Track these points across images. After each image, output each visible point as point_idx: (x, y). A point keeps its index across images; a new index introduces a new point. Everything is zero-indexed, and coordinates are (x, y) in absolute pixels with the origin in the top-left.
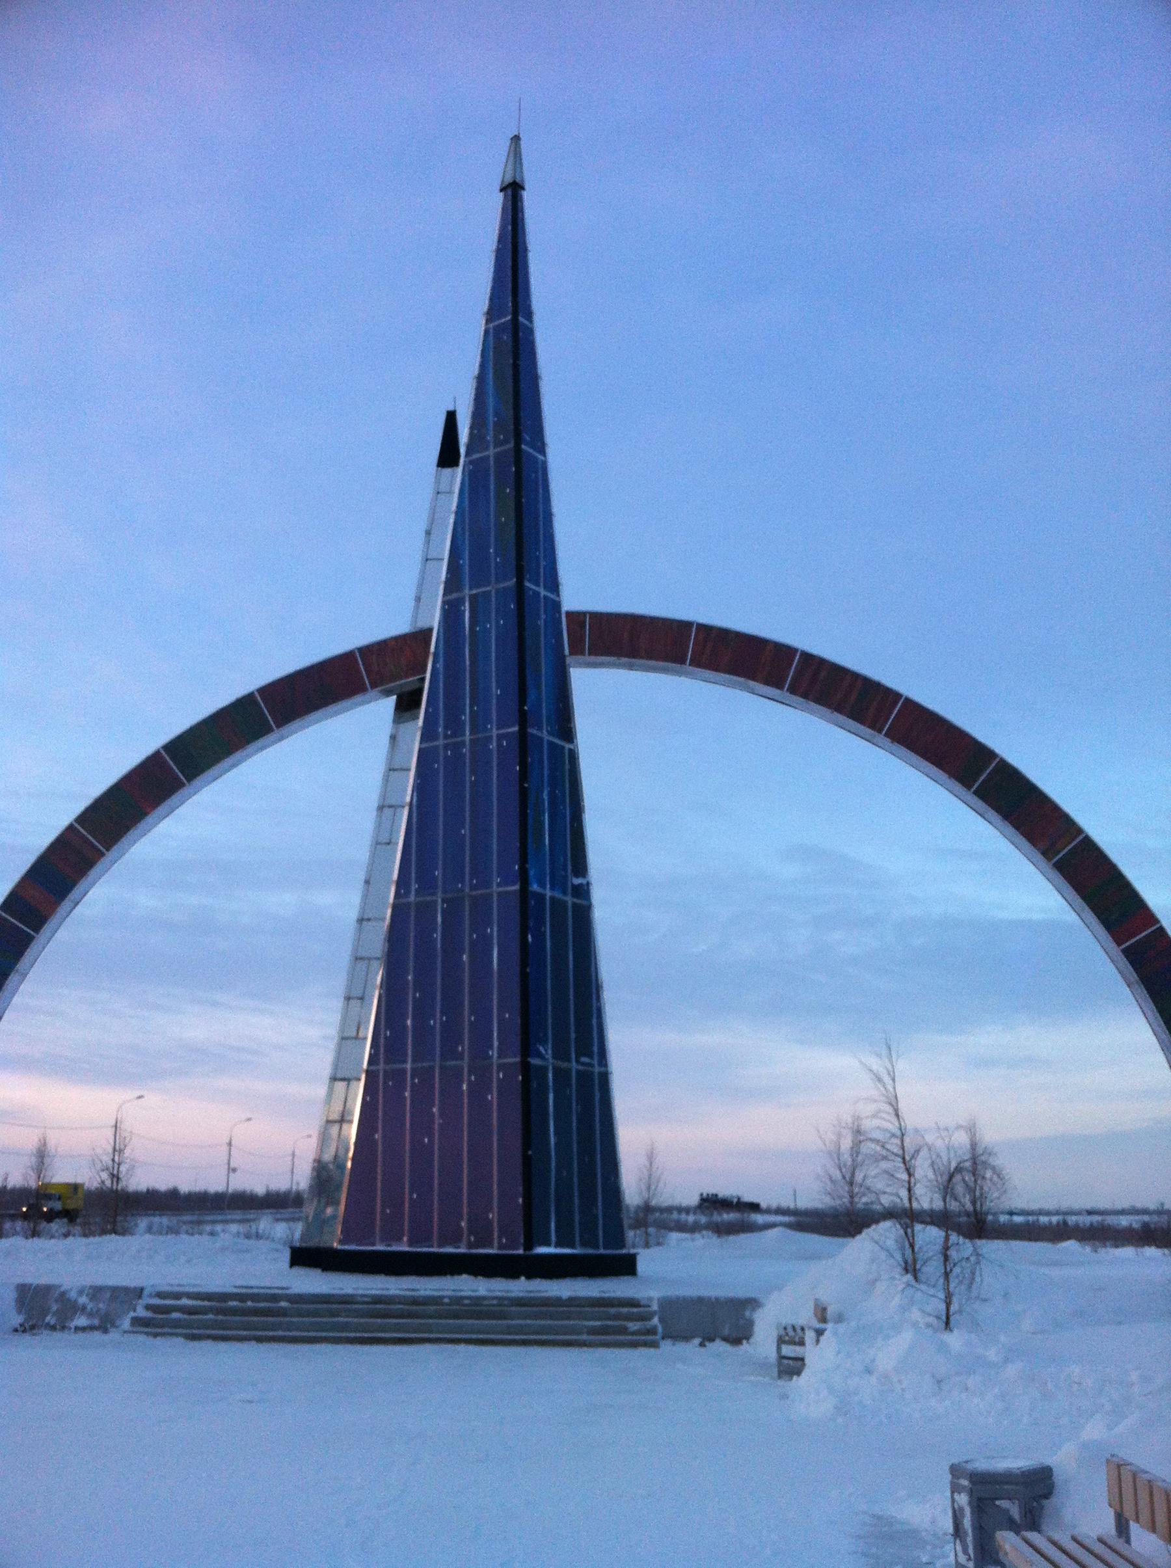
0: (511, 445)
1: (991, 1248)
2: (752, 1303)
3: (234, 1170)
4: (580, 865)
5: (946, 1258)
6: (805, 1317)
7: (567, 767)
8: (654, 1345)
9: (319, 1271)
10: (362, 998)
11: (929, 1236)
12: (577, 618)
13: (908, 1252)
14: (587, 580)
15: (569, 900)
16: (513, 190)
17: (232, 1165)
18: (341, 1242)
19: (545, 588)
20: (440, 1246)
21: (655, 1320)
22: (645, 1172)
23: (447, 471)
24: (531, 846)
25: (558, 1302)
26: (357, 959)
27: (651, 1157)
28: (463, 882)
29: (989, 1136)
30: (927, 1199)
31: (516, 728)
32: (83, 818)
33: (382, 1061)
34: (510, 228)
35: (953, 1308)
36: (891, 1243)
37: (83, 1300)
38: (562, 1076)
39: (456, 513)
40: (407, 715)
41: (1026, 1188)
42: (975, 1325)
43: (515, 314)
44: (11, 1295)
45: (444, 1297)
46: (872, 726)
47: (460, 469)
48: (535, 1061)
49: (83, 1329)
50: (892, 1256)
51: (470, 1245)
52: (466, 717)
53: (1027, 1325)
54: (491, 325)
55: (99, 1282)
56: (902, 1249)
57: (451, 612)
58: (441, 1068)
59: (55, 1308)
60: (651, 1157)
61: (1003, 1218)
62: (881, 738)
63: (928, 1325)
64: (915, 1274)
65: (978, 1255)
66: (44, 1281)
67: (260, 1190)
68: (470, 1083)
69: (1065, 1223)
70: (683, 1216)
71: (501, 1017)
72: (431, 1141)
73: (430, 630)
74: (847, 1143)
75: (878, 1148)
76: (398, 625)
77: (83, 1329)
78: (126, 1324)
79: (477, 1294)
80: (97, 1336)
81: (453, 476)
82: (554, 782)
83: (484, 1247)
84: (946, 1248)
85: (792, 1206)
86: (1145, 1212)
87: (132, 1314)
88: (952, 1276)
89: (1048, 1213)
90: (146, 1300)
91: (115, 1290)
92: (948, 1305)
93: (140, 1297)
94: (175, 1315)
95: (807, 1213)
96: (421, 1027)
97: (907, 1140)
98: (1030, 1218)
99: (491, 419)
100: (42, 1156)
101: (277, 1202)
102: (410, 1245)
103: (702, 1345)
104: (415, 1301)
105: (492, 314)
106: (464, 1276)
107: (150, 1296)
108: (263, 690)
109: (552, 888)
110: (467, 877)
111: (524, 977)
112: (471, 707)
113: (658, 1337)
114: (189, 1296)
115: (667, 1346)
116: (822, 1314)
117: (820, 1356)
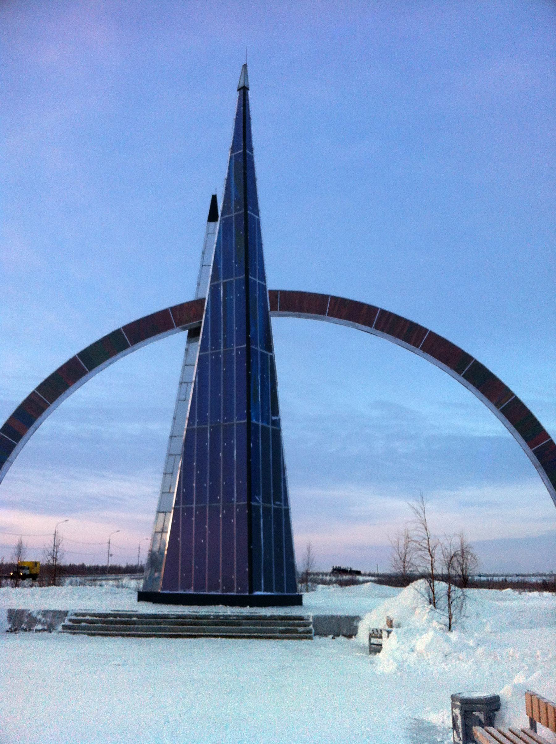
0: (243, 211)
1: (471, 592)
2: (357, 618)
3: (111, 555)
4: (275, 410)
5: (449, 597)
6: (382, 625)
7: (269, 364)
8: (311, 638)
9: (151, 603)
10: (172, 474)
11: (441, 587)
12: (274, 293)
13: (431, 594)
14: (279, 275)
15: (270, 427)
16: (244, 90)
17: (110, 553)
18: (162, 589)
19: (259, 279)
20: (209, 591)
21: (311, 627)
23: (212, 224)
24: (252, 402)
25: (265, 618)
26: (170, 455)
27: (309, 549)
28: (220, 419)
29: (469, 539)
30: (440, 569)
32: (39, 388)
33: (181, 503)
34: (242, 108)
35: (452, 621)
36: (423, 590)
37: (39, 617)
38: (267, 511)
39: (217, 243)
40: (193, 339)
41: (481, 567)
42: (463, 629)
43: (245, 149)
44: (5, 615)
46: (414, 345)
47: (218, 223)
48: (254, 504)
49: (40, 631)
52: (221, 340)
53: (488, 628)
54: (233, 154)
55: (47, 608)
56: (428, 592)
57: (214, 290)
58: (210, 507)
59: (26, 620)
60: (309, 549)
61: (476, 578)
62: (418, 350)
63: (441, 629)
64: (435, 605)
65: (464, 595)
66: (21, 608)
67: (124, 565)
68: (223, 514)
69: (506, 580)
70: (324, 577)
71: (238, 483)
73: (204, 299)
74: (402, 543)
75: (417, 545)
76: (189, 296)
77: (40, 631)
78: (60, 628)
79: (227, 614)
80: (46, 634)
81: (215, 226)
82: (263, 371)
83: (230, 592)
84: (449, 592)
85: (376, 572)
86: (544, 575)
87: (63, 624)
88: (452, 606)
89: (498, 576)
90: (70, 617)
92: (450, 619)
94: (83, 624)
99: (233, 199)
100: (20, 549)
102: (195, 591)
103: (333, 638)
104: (197, 617)
105: (234, 149)
106: (220, 605)
107: (71, 615)
108: (125, 328)
109: (262, 421)
111: (249, 464)
112: (224, 335)
114: (90, 615)
115: (317, 639)
116: (390, 623)
117: (389, 643)
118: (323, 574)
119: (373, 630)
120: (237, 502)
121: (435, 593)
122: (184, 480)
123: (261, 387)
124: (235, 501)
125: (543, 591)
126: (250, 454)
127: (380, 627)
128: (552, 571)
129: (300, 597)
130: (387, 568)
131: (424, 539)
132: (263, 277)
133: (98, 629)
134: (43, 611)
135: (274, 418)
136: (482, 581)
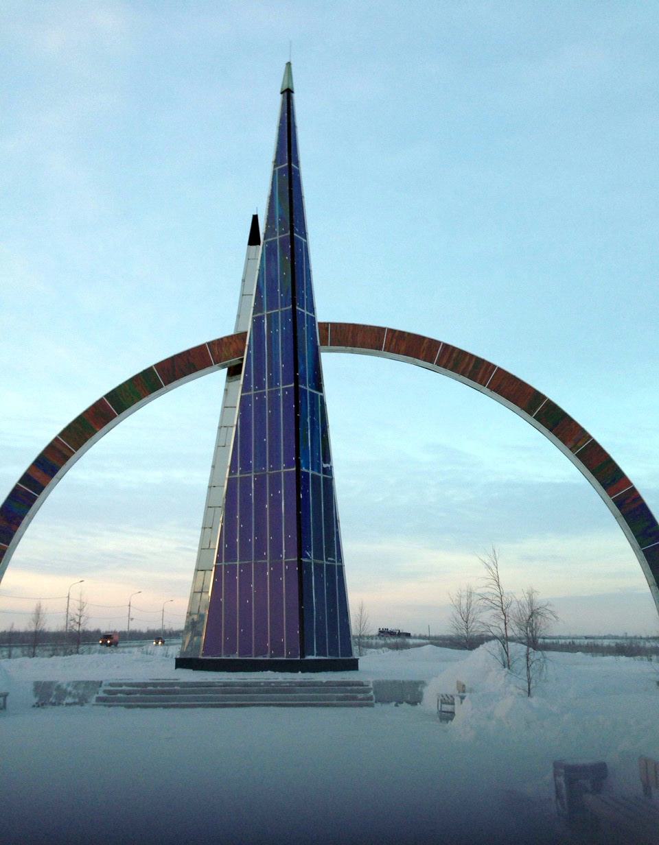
0: (289, 234)
2: (422, 683)
3: (132, 619)
4: (327, 457)
6: (452, 690)
7: (320, 405)
8: (372, 705)
9: (191, 670)
12: (324, 326)
13: (505, 656)
14: (330, 306)
15: (322, 475)
16: (288, 93)
17: (131, 616)
18: (203, 655)
19: (307, 310)
20: (255, 657)
21: (372, 693)
22: (359, 617)
23: (254, 247)
24: (301, 448)
25: (321, 684)
26: (208, 507)
27: (361, 610)
28: (265, 466)
29: (541, 598)
31: (293, 385)
32: (63, 434)
33: (223, 561)
34: (286, 114)
37: (69, 689)
38: (319, 567)
39: (259, 270)
40: (234, 378)
44: (31, 687)
45: (260, 682)
46: (480, 383)
47: (261, 247)
50: (497, 658)
51: (240, 655)
52: (266, 379)
54: (277, 168)
57: (257, 323)
58: (255, 563)
59: (55, 693)
60: (361, 610)
62: (485, 389)
63: (519, 694)
65: (545, 658)
66: (48, 679)
67: (144, 630)
69: (573, 643)
70: (370, 641)
71: (287, 535)
72: (250, 602)
73: (246, 333)
74: (464, 602)
75: (489, 603)
76: (229, 331)
78: (93, 701)
79: (278, 680)
80: (78, 707)
81: (257, 250)
82: (313, 413)
83: (280, 656)
85: (428, 635)
86: (616, 637)
87: (96, 695)
88: (530, 669)
89: (564, 638)
90: (103, 688)
91: (87, 683)
93: (100, 686)
94: (119, 695)
95: (435, 638)
96: (245, 544)
97: (504, 599)
98: (554, 641)
100: (38, 613)
101: (160, 637)
103: (396, 705)
104: (246, 685)
105: (277, 162)
106: (269, 672)
107: (105, 685)
108: (157, 365)
109: (313, 469)
110: (267, 464)
112: (268, 374)
113: (373, 702)
115: (378, 706)
116: (462, 688)
118: (368, 637)
119: (442, 696)
120: (285, 559)
121: (509, 655)
122: (226, 534)
123: (311, 431)
124: (284, 557)
125: (619, 655)
126: (301, 505)
127: (450, 692)
128: (626, 633)
129: (357, 660)
130: (444, 628)
131: (498, 596)
132: (312, 309)
133: (137, 700)
134: (74, 682)
135: (325, 466)
136: (547, 644)
